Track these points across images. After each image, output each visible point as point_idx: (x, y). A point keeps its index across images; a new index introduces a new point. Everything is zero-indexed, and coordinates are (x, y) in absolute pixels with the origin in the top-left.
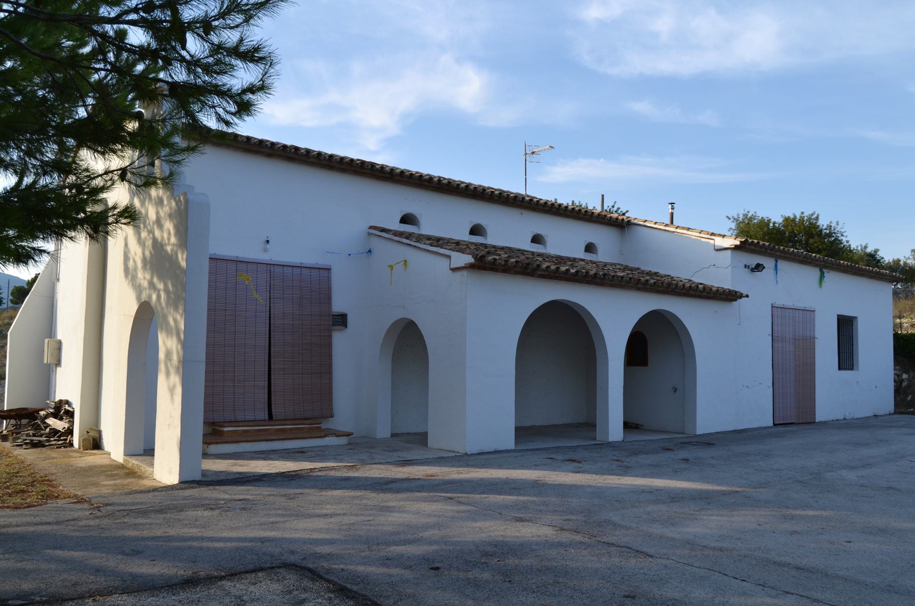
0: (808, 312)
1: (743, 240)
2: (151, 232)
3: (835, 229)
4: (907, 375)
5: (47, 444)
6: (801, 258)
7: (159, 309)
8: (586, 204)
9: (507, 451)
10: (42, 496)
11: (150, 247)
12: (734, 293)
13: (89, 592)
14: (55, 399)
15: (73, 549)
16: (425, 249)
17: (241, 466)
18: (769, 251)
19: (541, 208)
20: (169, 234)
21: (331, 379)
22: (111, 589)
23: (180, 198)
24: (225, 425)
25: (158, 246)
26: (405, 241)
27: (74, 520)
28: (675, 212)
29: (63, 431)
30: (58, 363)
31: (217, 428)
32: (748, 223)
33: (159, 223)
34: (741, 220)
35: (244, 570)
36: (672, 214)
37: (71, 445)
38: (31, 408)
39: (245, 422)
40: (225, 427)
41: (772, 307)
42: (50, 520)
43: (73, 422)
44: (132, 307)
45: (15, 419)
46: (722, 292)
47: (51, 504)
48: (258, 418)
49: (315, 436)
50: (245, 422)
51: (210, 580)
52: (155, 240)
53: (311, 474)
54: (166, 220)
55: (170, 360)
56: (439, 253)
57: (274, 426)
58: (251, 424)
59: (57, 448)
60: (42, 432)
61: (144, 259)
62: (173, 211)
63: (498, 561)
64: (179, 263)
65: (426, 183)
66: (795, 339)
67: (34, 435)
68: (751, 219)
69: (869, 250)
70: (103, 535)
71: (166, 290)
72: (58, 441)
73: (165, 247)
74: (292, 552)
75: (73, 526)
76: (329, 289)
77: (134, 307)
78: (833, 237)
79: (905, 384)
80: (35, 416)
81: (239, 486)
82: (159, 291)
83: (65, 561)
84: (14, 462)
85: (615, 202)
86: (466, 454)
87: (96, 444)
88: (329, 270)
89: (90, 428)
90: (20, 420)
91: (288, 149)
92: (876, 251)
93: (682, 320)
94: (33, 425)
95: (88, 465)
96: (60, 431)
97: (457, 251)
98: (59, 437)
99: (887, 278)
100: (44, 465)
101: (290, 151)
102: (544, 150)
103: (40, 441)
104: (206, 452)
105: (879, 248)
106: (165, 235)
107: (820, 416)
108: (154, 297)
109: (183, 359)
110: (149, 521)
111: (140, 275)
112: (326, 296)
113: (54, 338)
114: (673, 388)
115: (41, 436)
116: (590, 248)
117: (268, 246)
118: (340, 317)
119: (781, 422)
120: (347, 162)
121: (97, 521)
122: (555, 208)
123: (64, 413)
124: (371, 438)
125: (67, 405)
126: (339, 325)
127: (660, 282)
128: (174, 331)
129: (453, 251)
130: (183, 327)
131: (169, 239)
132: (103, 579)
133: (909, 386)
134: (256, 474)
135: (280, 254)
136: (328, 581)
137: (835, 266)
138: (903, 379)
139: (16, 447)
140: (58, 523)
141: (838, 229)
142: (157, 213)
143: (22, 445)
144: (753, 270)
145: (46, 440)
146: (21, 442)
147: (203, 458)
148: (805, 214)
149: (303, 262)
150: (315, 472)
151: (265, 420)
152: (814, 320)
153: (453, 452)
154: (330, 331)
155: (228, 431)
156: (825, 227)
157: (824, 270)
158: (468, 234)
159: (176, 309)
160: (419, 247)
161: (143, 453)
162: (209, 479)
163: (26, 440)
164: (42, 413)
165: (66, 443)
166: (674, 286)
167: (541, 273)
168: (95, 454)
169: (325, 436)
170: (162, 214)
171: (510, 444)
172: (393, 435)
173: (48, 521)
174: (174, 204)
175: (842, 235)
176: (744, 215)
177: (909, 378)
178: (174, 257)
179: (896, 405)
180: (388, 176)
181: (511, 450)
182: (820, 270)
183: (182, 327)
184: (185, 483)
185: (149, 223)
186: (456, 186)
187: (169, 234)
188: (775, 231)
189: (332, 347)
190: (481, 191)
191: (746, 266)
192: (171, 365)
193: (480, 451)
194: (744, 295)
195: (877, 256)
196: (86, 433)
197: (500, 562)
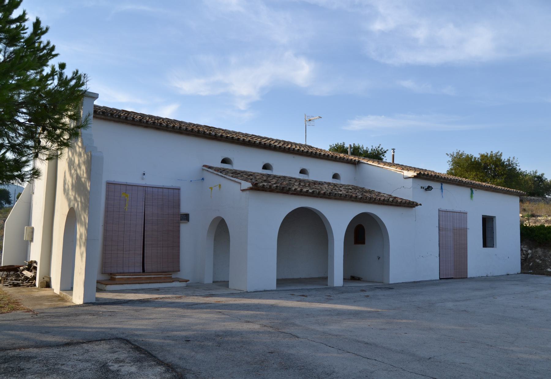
0: (463, 214)
1: (418, 173)
2: (76, 170)
3: (512, 162)
4: (531, 251)
5: (22, 285)
6: (456, 183)
7: (78, 211)
8: (363, 145)
9: (272, 291)
10: (11, 309)
11: (75, 178)
12: (412, 203)
13: (19, 347)
14: (29, 260)
15: (17, 331)
16: (229, 179)
17: (120, 296)
18: (435, 179)
19: (305, 154)
20: (83, 172)
21: (179, 250)
22: (29, 346)
23: (88, 154)
24: (117, 275)
25: (78, 178)
26: (220, 174)
27: (22, 319)
28: (395, 154)
29: (31, 278)
30: (32, 240)
31: (113, 276)
32: (460, 158)
33: (79, 165)
34: (455, 156)
35: (96, 340)
36: (393, 155)
37: (35, 285)
38: (16, 265)
39: (129, 273)
40: (116, 276)
41: (439, 211)
42: (10, 319)
43: (36, 273)
44: (67, 210)
45: (7, 272)
46: (404, 203)
47: (14, 312)
48: (136, 271)
49: (167, 281)
50: (129, 273)
51: (78, 343)
52: (77, 175)
53: (155, 300)
54: (82, 164)
55: (82, 239)
56: (235, 181)
57: (144, 275)
58: (132, 274)
59: (27, 287)
60: (20, 278)
61: (72, 185)
62: (85, 160)
63: (221, 338)
64: (87, 188)
65: (236, 141)
66: (454, 229)
67: (15, 280)
68: (462, 155)
69: (538, 174)
70: (34, 325)
71: (81, 202)
72: (28, 283)
73: (81, 179)
74: (123, 333)
75: (21, 321)
76: (179, 200)
77: (67, 210)
78: (511, 166)
79: (529, 256)
80: (18, 270)
81: (113, 305)
82: (78, 202)
83: (12, 335)
84: (1, 294)
85: (380, 145)
86: (247, 292)
87: (48, 285)
88: (179, 189)
89: (45, 276)
90: (9, 272)
91: (156, 123)
92: (543, 175)
93: (381, 218)
94: (16, 275)
95: (40, 295)
96: (29, 278)
97: (244, 181)
98: (28, 281)
99: (515, 193)
100: (17, 295)
101: (157, 125)
102: (316, 119)
103: (18, 283)
104: (105, 289)
105: (544, 173)
106: (82, 173)
107: (471, 273)
108: (76, 205)
109: (87, 238)
110: (59, 320)
111: (70, 193)
112: (177, 205)
113: (30, 226)
114: (378, 257)
115: (19, 281)
116: (335, 176)
117: (144, 177)
118: (185, 216)
119: (444, 277)
120: (190, 130)
121: (34, 320)
122: (313, 154)
123: (33, 268)
124: (201, 283)
125: (35, 264)
126: (184, 220)
127: (365, 197)
128: (84, 224)
129: (242, 180)
130: (87, 221)
131: (83, 175)
132: (27, 342)
133: (532, 257)
134: (125, 300)
135: (149, 181)
136: (133, 345)
137: (480, 187)
138: (529, 253)
139: (5, 286)
140: (14, 320)
141: (514, 162)
142: (79, 160)
143: (8, 285)
144: (426, 190)
145: (21, 283)
146: (7, 284)
147: (96, 292)
148: (493, 153)
149: (164, 185)
150: (158, 299)
151: (140, 273)
152: (466, 218)
153: (239, 290)
154: (179, 223)
155: (118, 278)
156: (506, 160)
157: (473, 189)
158: (262, 168)
159: (85, 212)
160: (226, 178)
161: (70, 289)
162: (100, 302)
163: (10, 282)
164: (21, 268)
165: (32, 284)
166: (373, 199)
167: (292, 192)
168: (46, 290)
169: (173, 282)
170: (81, 162)
171: (273, 286)
172: (213, 282)
173: (9, 319)
174: (86, 156)
175: (517, 165)
176: (457, 153)
177: (532, 252)
178: (85, 184)
179: (522, 268)
180: (214, 137)
181: (274, 290)
182: (471, 189)
183: (87, 221)
184: (86, 304)
185: (75, 166)
186: (253, 142)
187: (83, 172)
188: (475, 163)
189: (180, 232)
190: (269, 145)
191: (421, 187)
192: (82, 241)
193: (255, 291)
194: (418, 204)
195: (543, 178)
196: (42, 279)
197: (222, 339)
